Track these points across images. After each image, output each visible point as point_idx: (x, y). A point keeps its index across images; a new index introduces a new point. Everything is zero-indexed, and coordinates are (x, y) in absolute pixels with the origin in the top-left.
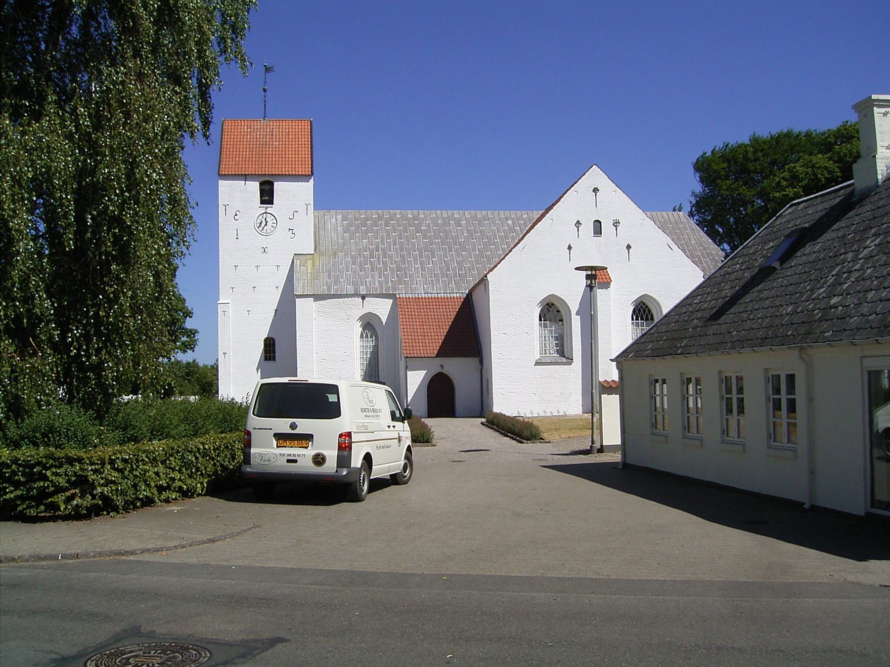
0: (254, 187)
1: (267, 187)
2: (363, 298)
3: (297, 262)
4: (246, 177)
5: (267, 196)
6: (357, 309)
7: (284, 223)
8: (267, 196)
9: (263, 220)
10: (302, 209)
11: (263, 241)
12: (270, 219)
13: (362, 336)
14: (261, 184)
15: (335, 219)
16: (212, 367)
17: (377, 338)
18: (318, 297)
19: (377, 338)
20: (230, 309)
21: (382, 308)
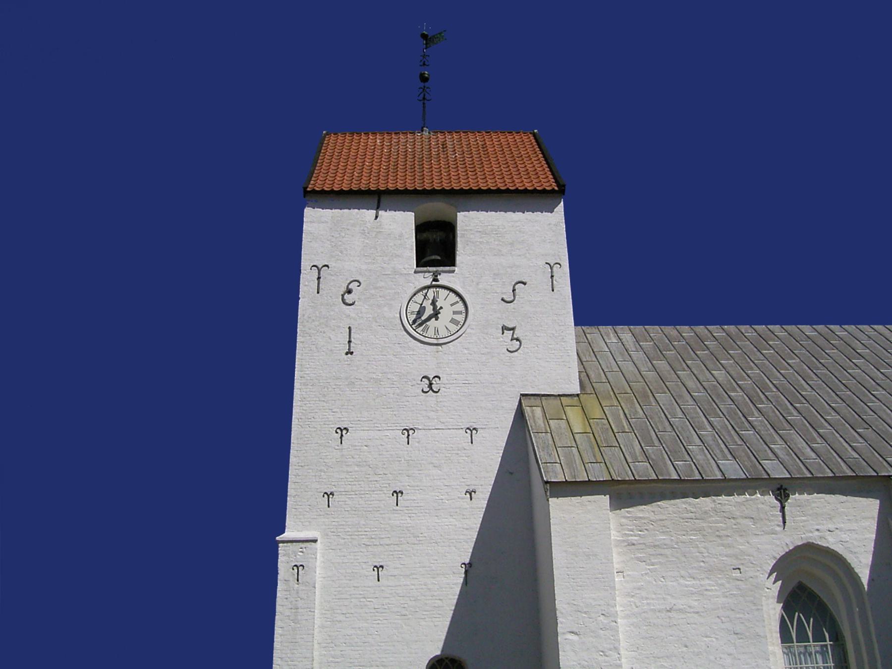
0: (400, 224)
1: (436, 236)
2: (782, 491)
3: (535, 414)
4: (377, 198)
5: (436, 246)
6: (759, 534)
7: (485, 310)
8: (436, 246)
9: (428, 304)
10: (539, 279)
11: (424, 359)
12: (445, 300)
13: (785, 636)
14: (421, 228)
15: (616, 340)
16: (787, 497)
17: (837, 637)
18: (626, 493)
19: (837, 637)
20: (319, 560)
21: (846, 527)
